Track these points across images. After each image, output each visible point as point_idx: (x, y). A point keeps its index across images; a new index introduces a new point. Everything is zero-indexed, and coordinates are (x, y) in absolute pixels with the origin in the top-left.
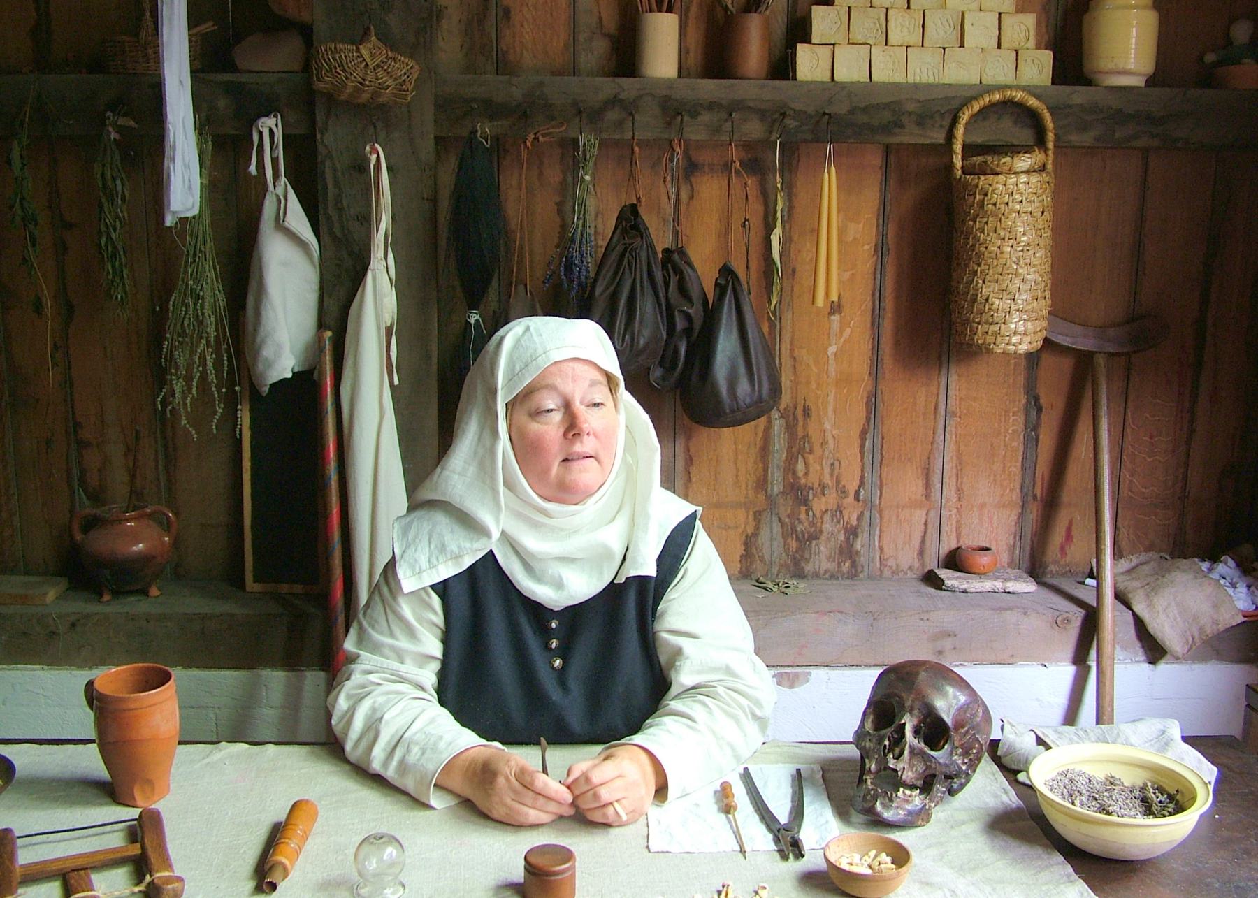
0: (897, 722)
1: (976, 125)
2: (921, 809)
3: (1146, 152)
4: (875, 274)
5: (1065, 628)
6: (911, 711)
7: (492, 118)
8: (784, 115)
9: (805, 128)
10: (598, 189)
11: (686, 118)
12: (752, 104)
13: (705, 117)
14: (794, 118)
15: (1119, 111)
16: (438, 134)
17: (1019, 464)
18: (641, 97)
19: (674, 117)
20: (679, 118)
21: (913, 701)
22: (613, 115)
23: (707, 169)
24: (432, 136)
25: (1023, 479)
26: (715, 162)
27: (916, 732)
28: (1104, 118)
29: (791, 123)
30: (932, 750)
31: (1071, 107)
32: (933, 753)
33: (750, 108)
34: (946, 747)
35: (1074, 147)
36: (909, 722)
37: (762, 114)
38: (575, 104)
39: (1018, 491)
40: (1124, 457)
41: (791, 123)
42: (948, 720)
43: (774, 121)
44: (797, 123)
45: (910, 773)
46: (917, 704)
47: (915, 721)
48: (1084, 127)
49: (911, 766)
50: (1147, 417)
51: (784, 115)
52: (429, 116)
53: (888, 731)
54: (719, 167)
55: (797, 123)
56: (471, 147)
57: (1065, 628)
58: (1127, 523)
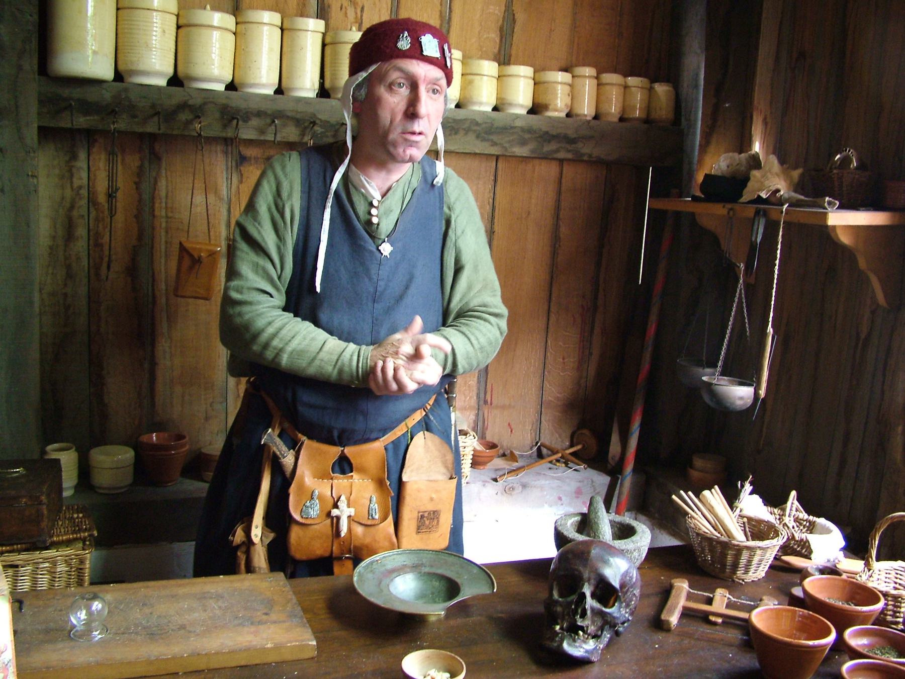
0: (579, 591)
1: (450, 137)
2: (594, 649)
3: (561, 161)
4: (115, 209)
5: (511, 494)
6: (589, 580)
7: (86, 114)
8: (314, 123)
9: (329, 134)
10: (169, 173)
11: (240, 123)
12: (289, 114)
13: (254, 122)
14: (321, 126)
15: (547, 133)
16: (41, 124)
17: (476, 379)
18: (205, 104)
19: (231, 121)
20: (235, 122)
21: (589, 573)
22: (184, 116)
23: (253, 162)
24: (36, 125)
25: (479, 389)
26: (259, 156)
27: (593, 596)
28: (537, 137)
29: (318, 129)
30: (606, 607)
31: (515, 127)
32: (607, 610)
33: (288, 117)
34: (616, 604)
35: (517, 156)
36: (587, 590)
37: (298, 122)
38: (153, 106)
39: (475, 398)
40: (546, 373)
41: (318, 129)
42: (616, 584)
43: (305, 128)
44: (323, 130)
45: (592, 627)
46: (593, 576)
47: (592, 588)
48: (523, 143)
49: (593, 622)
50: (561, 346)
51: (314, 123)
52: (34, 108)
53: (574, 597)
54: (262, 160)
55: (323, 130)
56: (732, 225)
57: (511, 494)
58: (548, 418)
